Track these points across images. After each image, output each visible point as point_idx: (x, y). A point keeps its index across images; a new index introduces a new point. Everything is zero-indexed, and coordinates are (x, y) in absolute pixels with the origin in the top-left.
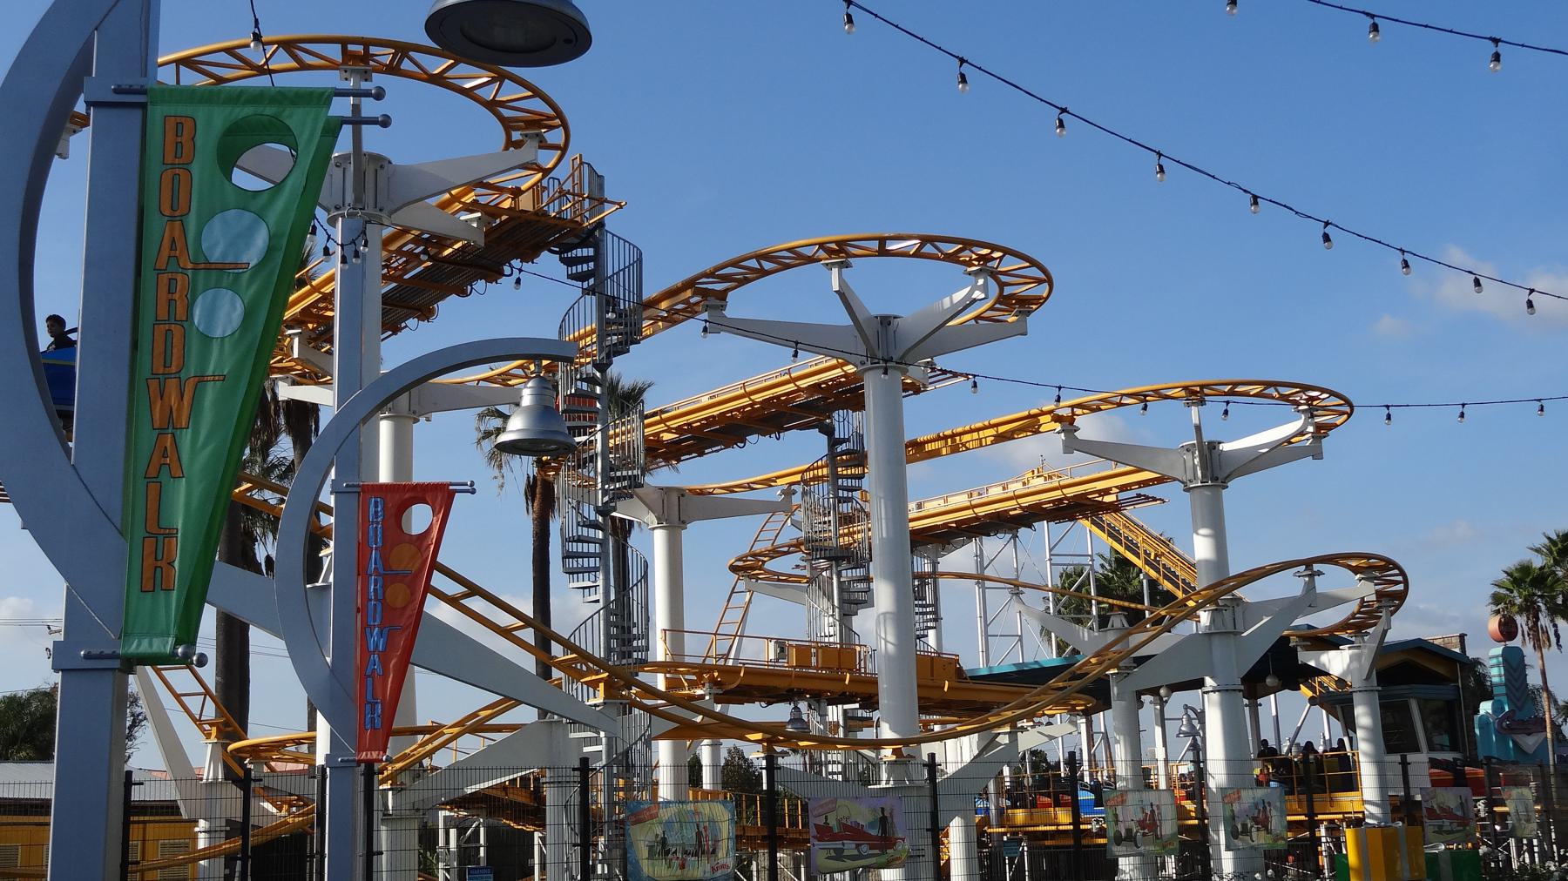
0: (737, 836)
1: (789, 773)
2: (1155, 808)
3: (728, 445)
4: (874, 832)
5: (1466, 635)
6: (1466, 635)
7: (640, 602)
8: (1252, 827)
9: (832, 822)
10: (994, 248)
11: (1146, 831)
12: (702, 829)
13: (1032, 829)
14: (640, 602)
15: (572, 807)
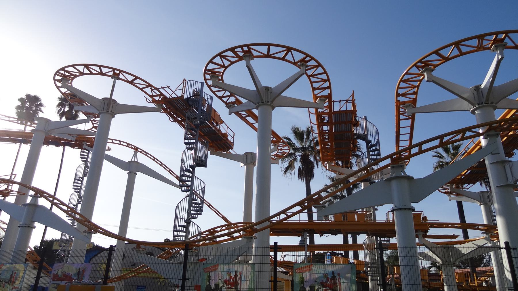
0: (457, 285)
1: (154, 259)
2: (238, 274)
3: (72, 147)
7: (375, 137)
8: (223, 286)
9: (60, 273)
10: (497, 33)
11: (230, 286)
12: (13, 274)
14: (375, 137)
15: (119, 270)
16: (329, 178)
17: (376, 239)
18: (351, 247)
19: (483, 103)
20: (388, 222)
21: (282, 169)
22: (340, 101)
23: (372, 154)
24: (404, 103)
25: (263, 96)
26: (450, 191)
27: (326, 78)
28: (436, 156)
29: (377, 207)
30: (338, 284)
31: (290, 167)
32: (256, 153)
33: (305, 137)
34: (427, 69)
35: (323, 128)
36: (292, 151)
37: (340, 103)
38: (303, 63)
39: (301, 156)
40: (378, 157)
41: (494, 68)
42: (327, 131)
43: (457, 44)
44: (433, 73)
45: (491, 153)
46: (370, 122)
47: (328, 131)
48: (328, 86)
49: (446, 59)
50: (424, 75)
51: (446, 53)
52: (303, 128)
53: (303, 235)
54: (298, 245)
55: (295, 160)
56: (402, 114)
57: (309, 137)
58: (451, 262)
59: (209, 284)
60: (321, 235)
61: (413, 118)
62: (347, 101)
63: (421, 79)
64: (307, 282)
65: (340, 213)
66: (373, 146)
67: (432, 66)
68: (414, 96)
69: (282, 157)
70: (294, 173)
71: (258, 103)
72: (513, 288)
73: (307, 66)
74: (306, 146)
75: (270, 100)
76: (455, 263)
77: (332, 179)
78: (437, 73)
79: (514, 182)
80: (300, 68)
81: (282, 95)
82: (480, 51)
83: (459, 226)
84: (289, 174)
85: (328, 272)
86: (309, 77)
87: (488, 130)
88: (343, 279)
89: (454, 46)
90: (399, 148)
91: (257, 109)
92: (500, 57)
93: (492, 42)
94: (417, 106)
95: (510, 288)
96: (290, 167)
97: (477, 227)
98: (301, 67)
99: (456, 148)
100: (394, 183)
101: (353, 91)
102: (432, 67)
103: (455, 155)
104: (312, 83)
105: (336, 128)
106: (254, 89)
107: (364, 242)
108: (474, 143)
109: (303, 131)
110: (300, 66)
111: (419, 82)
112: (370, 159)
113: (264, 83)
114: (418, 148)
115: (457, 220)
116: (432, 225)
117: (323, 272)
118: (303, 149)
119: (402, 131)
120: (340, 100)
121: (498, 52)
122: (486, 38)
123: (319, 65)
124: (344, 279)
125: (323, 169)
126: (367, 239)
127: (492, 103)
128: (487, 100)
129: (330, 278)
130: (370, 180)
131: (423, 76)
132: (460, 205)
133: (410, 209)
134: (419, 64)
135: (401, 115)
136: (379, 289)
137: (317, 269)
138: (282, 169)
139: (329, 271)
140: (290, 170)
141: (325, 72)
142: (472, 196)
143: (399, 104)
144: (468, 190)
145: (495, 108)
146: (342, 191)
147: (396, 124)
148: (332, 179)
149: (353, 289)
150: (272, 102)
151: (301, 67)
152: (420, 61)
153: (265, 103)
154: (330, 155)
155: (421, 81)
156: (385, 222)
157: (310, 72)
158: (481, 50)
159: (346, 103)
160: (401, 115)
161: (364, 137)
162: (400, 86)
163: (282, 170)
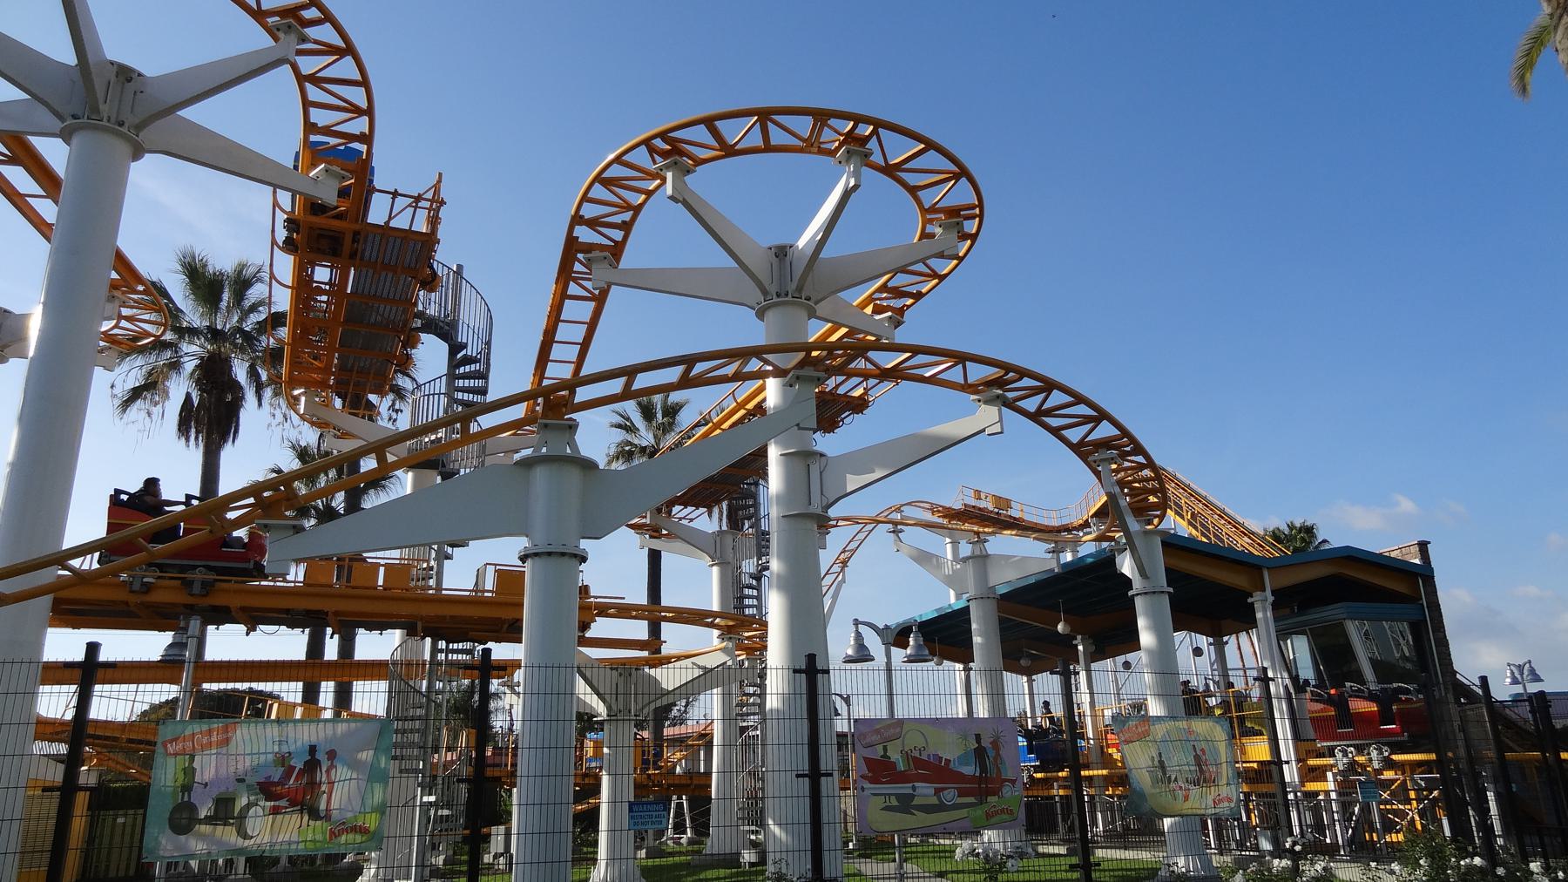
4: (969, 770)
5: (1429, 543)
6: (1429, 543)
7: (480, 336)
9: (895, 756)
10: (858, 119)
13: (232, 431)
14: (480, 336)
16: (293, 447)
17: (434, 645)
18: (330, 670)
19: (790, 295)
20: (479, 594)
21: (117, 390)
22: (395, 194)
23: (461, 385)
24: (589, 248)
25: (100, 94)
26: (648, 523)
27: (364, 105)
28: (619, 426)
29: (449, 550)
30: (324, 788)
31: (149, 388)
32: (23, 318)
33: (226, 296)
34: (676, 163)
35: (313, 272)
36: (169, 336)
37: (393, 199)
38: (291, 20)
39: (202, 358)
40: (477, 398)
41: (828, 213)
42: (325, 284)
43: (765, 116)
44: (688, 179)
45: (798, 425)
46: (472, 286)
47: (327, 288)
48: (363, 134)
49: (729, 151)
50: (664, 180)
51: (735, 131)
52: (222, 261)
53: (182, 624)
54: (159, 658)
55: (175, 366)
56: (575, 280)
57: (243, 299)
58: (630, 711)
59: (186, 799)
60: (251, 629)
61: (600, 299)
62: (418, 198)
63: (650, 188)
64: (206, 785)
65: (329, 558)
66: (468, 360)
67: (690, 157)
68: (618, 235)
69: (127, 347)
70: (160, 415)
71: (74, 117)
72: (807, 772)
73: (304, 39)
74: (228, 326)
75: (130, 120)
76: (639, 716)
77: (303, 454)
78: (701, 182)
79: (822, 508)
80: (276, 39)
81: (187, 113)
82: (810, 152)
83: (671, 615)
84: (143, 414)
85: (292, 749)
86: (301, 79)
87: (801, 365)
88: (345, 769)
89: (756, 118)
90: (542, 377)
91: (66, 136)
92: (852, 183)
93: (842, 138)
94: (621, 266)
95: (802, 772)
96: (149, 388)
97: (710, 620)
98: (281, 35)
99: (672, 411)
100: (540, 474)
101: (440, 174)
102: (690, 162)
103: (666, 428)
104: (307, 104)
105: (362, 280)
106: (68, 57)
107: (393, 654)
108: (736, 401)
109: (222, 274)
110: (278, 30)
111: (643, 197)
112: (453, 401)
113: (116, 46)
114: (623, 380)
115: (641, 598)
116: (604, 610)
117: (276, 749)
118: (214, 334)
119: (563, 332)
120: (396, 190)
121: (849, 168)
122: (832, 122)
123: (349, 50)
124: (350, 767)
125: (274, 415)
126: (399, 649)
127: (808, 299)
128: (800, 289)
129: (299, 765)
130: (444, 466)
131: (658, 181)
132: (655, 558)
133: (575, 556)
134: (658, 143)
135: (572, 284)
136: (419, 798)
137: (254, 736)
138: (117, 390)
139: (299, 743)
140: (148, 401)
141: (364, 83)
142: (695, 541)
143: (572, 247)
144: (691, 524)
145: (812, 314)
146: (329, 497)
147: (551, 307)
148: (303, 454)
149: (376, 800)
150: (139, 128)
151: (281, 35)
152: (663, 135)
153: (105, 123)
154: (320, 368)
155: (649, 193)
156: (468, 593)
157: (308, 65)
158: (814, 153)
159: (410, 205)
160: (572, 284)
161: (447, 328)
162: (590, 195)
163: (114, 396)
